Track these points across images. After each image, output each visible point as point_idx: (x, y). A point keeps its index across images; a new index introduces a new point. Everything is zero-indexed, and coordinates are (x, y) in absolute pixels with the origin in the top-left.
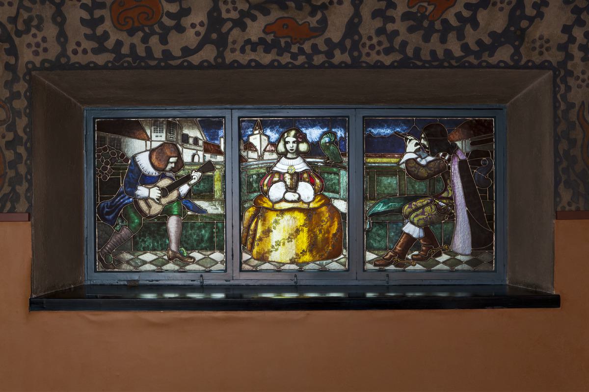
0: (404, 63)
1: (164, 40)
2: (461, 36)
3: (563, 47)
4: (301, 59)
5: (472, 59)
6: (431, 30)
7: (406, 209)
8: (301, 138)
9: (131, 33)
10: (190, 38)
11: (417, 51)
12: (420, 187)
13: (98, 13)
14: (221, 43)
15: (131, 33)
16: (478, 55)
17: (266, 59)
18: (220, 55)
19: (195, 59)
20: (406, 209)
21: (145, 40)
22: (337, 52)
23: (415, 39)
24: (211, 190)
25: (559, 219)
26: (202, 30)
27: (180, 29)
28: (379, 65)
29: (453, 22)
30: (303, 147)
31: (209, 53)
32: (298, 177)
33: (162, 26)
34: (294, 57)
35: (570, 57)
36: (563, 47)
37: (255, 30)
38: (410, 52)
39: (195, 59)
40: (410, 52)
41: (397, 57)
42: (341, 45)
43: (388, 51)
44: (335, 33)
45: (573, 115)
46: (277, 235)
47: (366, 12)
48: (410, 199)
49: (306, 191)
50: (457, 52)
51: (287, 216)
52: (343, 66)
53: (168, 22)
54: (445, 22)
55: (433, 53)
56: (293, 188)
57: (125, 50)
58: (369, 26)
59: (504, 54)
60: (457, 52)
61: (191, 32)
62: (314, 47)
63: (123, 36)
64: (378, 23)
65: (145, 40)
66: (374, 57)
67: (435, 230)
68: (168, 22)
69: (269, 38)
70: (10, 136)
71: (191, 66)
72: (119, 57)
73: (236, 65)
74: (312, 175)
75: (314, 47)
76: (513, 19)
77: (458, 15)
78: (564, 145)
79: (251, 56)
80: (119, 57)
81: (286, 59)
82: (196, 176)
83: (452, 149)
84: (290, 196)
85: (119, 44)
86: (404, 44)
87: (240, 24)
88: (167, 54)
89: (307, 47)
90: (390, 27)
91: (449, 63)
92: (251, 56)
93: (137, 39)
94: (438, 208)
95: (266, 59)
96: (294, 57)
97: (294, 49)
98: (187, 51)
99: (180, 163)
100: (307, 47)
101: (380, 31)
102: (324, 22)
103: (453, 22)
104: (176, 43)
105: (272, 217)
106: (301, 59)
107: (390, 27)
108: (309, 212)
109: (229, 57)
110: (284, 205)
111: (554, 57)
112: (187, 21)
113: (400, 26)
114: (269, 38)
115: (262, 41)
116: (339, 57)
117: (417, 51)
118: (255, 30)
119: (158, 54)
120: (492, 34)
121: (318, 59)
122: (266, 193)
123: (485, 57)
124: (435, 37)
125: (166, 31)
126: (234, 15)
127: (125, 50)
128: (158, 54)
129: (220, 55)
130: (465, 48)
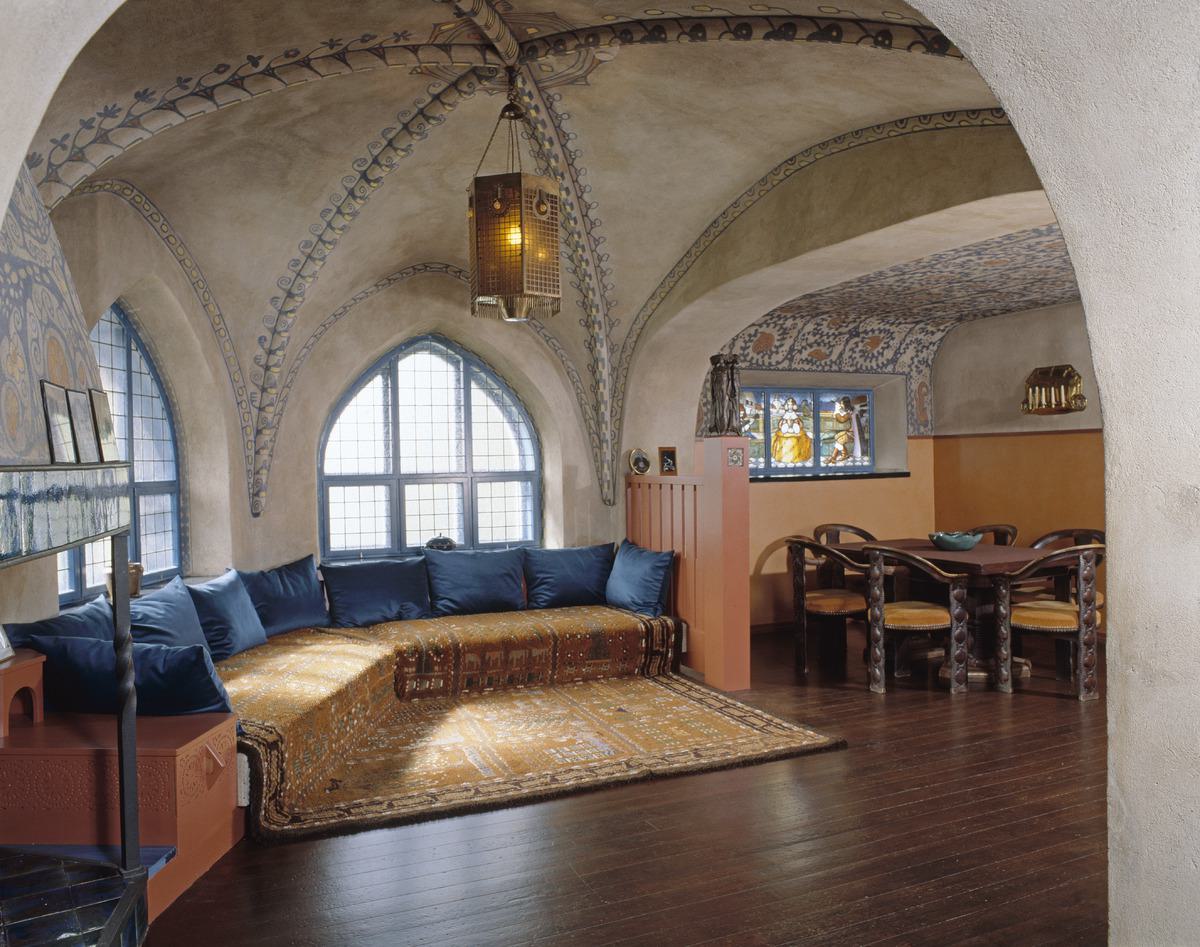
0: (856, 371)
1: (770, 358)
2: (877, 360)
3: (910, 366)
4: (820, 368)
5: (879, 370)
6: (867, 357)
7: (836, 437)
8: (794, 402)
9: (758, 354)
10: (780, 357)
11: (861, 365)
12: (841, 426)
13: (748, 345)
14: (791, 360)
15: (758, 354)
16: (881, 368)
17: (807, 367)
18: (790, 365)
19: (780, 367)
20: (836, 437)
21: (762, 357)
22: (833, 365)
23: (861, 361)
24: (758, 428)
25: (1103, 423)
26: (785, 354)
27: (777, 353)
28: (848, 372)
29: (876, 354)
30: (795, 407)
31: (786, 364)
32: (793, 421)
33: (770, 350)
34: (818, 367)
35: (912, 370)
36: (910, 366)
37: (805, 354)
38: (859, 366)
39: (780, 367)
40: (859, 366)
41: (854, 368)
42: (835, 363)
43: (851, 366)
44: (834, 357)
45: (913, 395)
46: (784, 450)
47: (847, 349)
48: (837, 432)
49: (796, 428)
50: (875, 367)
51: (789, 440)
52: (836, 371)
53: (774, 349)
54: (873, 354)
55: (867, 367)
56: (791, 427)
57: (754, 361)
58: (847, 354)
59: (890, 368)
60: (875, 367)
61: (781, 354)
62: (826, 363)
63: (755, 355)
64: (850, 353)
65: (762, 357)
66: (846, 369)
67: (847, 446)
68: (774, 349)
69: (809, 358)
70: (705, 400)
71: (778, 370)
72: (751, 364)
73: (796, 370)
74: (799, 421)
75: (826, 363)
76: (896, 353)
77: (878, 352)
78: (910, 408)
79: (801, 366)
80: (751, 364)
81: (814, 368)
82: (752, 420)
83: (852, 409)
84: (791, 430)
85: (752, 358)
86: (857, 363)
87: (800, 352)
88: (770, 364)
89: (823, 363)
90: (854, 355)
91: (42, 277)
92: (801, 366)
93: (759, 357)
94: (848, 436)
95: (807, 367)
96: (818, 367)
97: (818, 363)
98: (778, 363)
99: (745, 415)
100: (823, 363)
101: (850, 357)
102: (831, 352)
103: (876, 354)
104: (775, 358)
105: (784, 440)
106: (820, 368)
107: (854, 355)
108: (798, 439)
109: (794, 366)
110: (788, 435)
111: (907, 370)
112: (780, 350)
113: (857, 355)
114: (809, 358)
115: (806, 359)
116: (835, 368)
117: (861, 365)
118: (805, 354)
119: (767, 364)
120: (888, 360)
121: (827, 368)
122: (780, 429)
123: (884, 369)
124: (868, 360)
125: (772, 353)
126: (800, 348)
127: (754, 361)
128: (767, 364)
129: (790, 365)
130: (878, 365)
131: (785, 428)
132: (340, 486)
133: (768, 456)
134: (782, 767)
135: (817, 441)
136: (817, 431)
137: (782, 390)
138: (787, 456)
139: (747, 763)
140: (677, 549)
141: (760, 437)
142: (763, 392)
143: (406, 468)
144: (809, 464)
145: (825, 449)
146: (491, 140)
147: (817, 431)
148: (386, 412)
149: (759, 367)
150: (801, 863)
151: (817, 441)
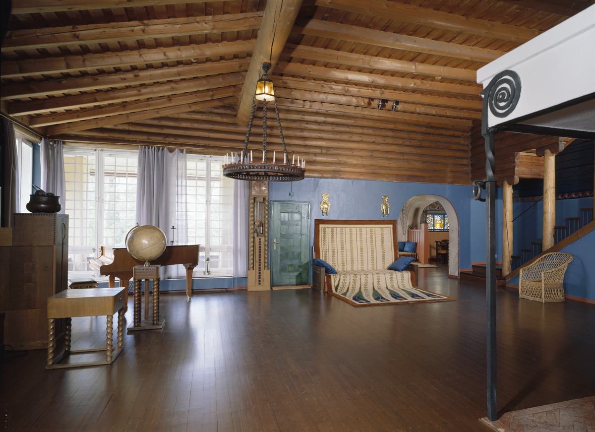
49: (440, 222)
131: (437, 221)
132: (65, 202)
133: (434, 227)
134: (423, 269)
135: (444, 224)
136: (444, 222)
137: (437, 214)
138: (438, 227)
139: (121, 352)
140: (417, 242)
141: (432, 223)
142: (433, 215)
143: (195, 188)
144: (442, 228)
145: (446, 226)
146: (240, 19)
147: (444, 222)
148: (192, 179)
149: (432, 210)
150: (106, 292)
151: (444, 224)
